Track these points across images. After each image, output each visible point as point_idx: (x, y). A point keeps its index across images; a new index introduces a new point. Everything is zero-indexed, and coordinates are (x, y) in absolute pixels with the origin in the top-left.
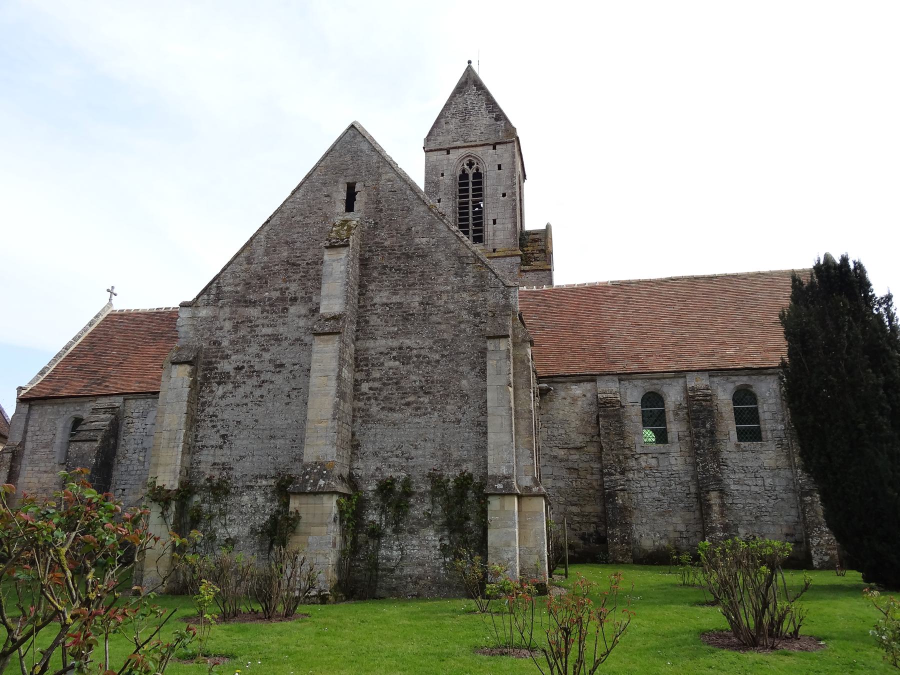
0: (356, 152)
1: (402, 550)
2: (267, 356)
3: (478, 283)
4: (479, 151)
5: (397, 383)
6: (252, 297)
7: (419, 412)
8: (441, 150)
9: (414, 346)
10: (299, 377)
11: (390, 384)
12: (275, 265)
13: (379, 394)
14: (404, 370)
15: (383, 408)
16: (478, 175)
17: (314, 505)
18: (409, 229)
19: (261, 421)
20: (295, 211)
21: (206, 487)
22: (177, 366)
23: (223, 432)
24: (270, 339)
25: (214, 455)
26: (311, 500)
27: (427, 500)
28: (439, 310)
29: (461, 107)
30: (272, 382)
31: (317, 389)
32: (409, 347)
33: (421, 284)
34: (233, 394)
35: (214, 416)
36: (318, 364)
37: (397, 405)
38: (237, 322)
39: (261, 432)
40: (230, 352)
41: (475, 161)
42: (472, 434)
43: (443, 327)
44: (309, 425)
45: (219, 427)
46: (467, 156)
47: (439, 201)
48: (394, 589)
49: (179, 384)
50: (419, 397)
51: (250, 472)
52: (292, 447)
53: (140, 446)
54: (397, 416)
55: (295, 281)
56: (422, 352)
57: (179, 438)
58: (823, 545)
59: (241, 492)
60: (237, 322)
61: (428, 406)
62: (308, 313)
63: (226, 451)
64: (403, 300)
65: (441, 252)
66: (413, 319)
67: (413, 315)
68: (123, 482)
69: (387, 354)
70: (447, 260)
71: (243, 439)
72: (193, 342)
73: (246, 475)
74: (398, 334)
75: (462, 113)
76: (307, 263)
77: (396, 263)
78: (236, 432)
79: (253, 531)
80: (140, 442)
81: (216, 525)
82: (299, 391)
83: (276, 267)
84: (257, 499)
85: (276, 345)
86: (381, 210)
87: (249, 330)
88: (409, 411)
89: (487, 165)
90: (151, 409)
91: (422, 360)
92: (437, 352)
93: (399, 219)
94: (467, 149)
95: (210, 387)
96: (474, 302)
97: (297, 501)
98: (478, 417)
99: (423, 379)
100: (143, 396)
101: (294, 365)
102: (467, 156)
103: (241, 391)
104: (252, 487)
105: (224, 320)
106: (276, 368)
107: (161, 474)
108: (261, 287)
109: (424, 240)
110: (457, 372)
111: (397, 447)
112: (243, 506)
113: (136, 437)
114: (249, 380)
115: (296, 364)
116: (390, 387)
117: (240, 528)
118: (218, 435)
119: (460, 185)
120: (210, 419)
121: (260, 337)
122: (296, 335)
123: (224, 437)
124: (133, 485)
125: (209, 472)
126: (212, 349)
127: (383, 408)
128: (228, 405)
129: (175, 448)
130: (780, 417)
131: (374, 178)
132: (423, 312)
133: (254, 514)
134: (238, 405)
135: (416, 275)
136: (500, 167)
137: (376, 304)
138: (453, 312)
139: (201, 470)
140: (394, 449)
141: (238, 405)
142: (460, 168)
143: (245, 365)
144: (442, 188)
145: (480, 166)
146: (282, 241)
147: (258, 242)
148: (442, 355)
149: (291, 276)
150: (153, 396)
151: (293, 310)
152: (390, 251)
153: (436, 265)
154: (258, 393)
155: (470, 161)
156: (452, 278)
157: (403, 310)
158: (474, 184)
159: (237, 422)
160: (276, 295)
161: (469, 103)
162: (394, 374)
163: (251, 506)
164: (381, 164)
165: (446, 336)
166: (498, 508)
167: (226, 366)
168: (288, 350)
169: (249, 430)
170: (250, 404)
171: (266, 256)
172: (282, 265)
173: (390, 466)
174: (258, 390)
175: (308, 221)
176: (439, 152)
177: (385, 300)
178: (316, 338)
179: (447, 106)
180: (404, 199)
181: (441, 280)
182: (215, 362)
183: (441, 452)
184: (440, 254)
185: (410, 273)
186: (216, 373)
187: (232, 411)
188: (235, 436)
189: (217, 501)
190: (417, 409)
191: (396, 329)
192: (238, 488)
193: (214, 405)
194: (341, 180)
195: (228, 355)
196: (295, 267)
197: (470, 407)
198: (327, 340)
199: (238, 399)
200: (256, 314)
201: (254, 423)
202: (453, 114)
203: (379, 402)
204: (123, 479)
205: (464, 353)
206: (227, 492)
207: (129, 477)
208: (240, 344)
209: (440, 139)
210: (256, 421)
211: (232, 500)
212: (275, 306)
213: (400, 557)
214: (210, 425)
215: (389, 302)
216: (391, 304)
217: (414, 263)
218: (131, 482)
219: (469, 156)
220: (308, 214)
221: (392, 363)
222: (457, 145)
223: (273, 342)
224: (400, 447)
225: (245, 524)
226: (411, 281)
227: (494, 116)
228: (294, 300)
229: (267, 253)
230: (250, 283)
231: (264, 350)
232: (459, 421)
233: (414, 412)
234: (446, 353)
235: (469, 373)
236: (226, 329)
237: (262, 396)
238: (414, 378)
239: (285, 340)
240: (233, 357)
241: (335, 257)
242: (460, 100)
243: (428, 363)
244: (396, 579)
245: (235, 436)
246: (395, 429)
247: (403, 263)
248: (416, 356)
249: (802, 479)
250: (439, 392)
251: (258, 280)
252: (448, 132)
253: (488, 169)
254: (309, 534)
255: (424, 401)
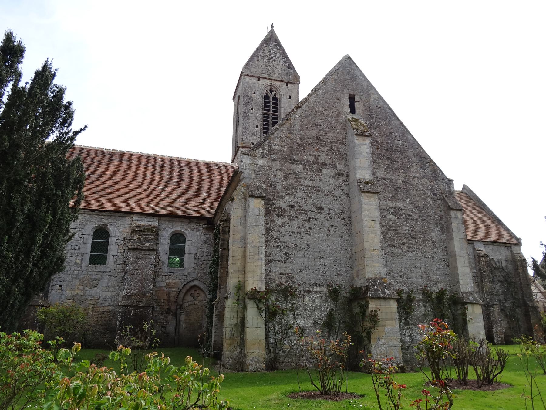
0: (353, 75)
1: (411, 336)
2: (310, 200)
3: (433, 175)
4: (278, 84)
5: (396, 230)
6: (295, 157)
7: (410, 250)
8: (254, 77)
9: (403, 207)
10: (334, 218)
11: (391, 230)
12: (309, 138)
13: (386, 236)
14: (398, 222)
15: (389, 245)
16: (275, 99)
17: (385, 307)
18: (391, 133)
19: (311, 246)
20: (317, 104)
21: (277, 290)
22: (254, 199)
23: (285, 251)
24: (311, 189)
25: (281, 267)
26: (382, 303)
27: (421, 305)
28: (414, 188)
29: (267, 53)
30: (316, 219)
31: (368, 229)
32: (400, 208)
33: (402, 169)
34: (290, 224)
35: (277, 239)
36: (366, 212)
37: (397, 244)
38: (286, 173)
39: (312, 253)
40: (283, 194)
41: (275, 90)
42: (441, 266)
43: (418, 198)
44: (366, 252)
45: (282, 247)
46: (270, 85)
47: (252, 109)
48: (409, 361)
49: (257, 212)
50: (409, 240)
51: (307, 281)
52: (335, 266)
53: (77, 251)
54: (397, 251)
55: (323, 152)
56: (408, 212)
57: (262, 253)
58: (498, 332)
59: (303, 295)
60: (286, 173)
61: (415, 247)
62: (335, 176)
63: (288, 264)
64: (393, 178)
65: (411, 152)
66: (400, 191)
67: (400, 188)
68: (60, 279)
69: (387, 210)
70: (415, 157)
71: (301, 257)
72: (255, 182)
73: (305, 283)
74: (392, 199)
75: (268, 57)
76: (330, 142)
77: (386, 153)
78: (294, 252)
79: (315, 323)
80: (77, 248)
81: (289, 318)
82: (335, 227)
83: (310, 140)
84: (315, 300)
85: (316, 193)
86: (373, 117)
87: (295, 180)
88: (404, 248)
89: (282, 94)
90: (88, 223)
91: (409, 218)
92: (416, 213)
93: (385, 126)
94: (270, 81)
95: (271, 217)
96: (432, 186)
97: (373, 304)
98: (442, 256)
99: (410, 229)
100: (98, 213)
101: (330, 209)
102: (270, 85)
103: (295, 223)
104: (311, 292)
105: (277, 170)
106: (318, 210)
107: (250, 278)
108: (301, 151)
109: (400, 142)
110: (428, 227)
111: (400, 270)
112: (306, 305)
113: (73, 244)
114: (300, 216)
115: (331, 209)
116: (392, 232)
117: (306, 320)
118: (282, 253)
119: (265, 102)
120: (275, 241)
121: (304, 187)
122: (329, 189)
123: (286, 254)
124: (71, 282)
125: (277, 279)
126: (269, 189)
127: (389, 245)
128: (287, 232)
129: (260, 260)
130: (474, 266)
131: (366, 95)
132: (405, 187)
133: (314, 310)
134: (294, 233)
135: (399, 164)
136: (290, 97)
137: (377, 177)
138: (422, 190)
139: (272, 277)
140: (399, 272)
141: (294, 233)
142: (265, 92)
143: (296, 204)
144: (254, 101)
145: (278, 94)
146: (312, 123)
147: (294, 119)
148: (419, 216)
149: (320, 148)
150: (92, 213)
151: (324, 171)
152: (381, 145)
153: (409, 159)
154: (307, 225)
155: (271, 88)
156: (419, 169)
157: (394, 184)
158: (273, 104)
159: (295, 245)
160: (312, 159)
161: (272, 52)
162: (393, 224)
163: (312, 305)
164: (369, 87)
165: (420, 204)
166: (471, 311)
167: (281, 203)
168: (324, 199)
169: (304, 251)
170: (302, 233)
171: (301, 130)
172: (314, 139)
173: (397, 282)
174: (307, 223)
175: (326, 112)
176: (253, 78)
177: (382, 176)
178: (363, 194)
179: (258, 50)
180: (386, 114)
181: (413, 169)
182: (273, 200)
183: (425, 276)
184: (410, 153)
185: (395, 161)
186: (275, 208)
187: (290, 237)
188: (295, 255)
189: (286, 300)
190: (409, 247)
191: (391, 195)
192: (300, 292)
193: (276, 230)
194: (346, 91)
195: (282, 196)
196: (322, 142)
197: (438, 250)
198: (371, 197)
199: (293, 229)
200: (299, 170)
201: (307, 246)
202: (262, 56)
203: (386, 241)
204: (60, 277)
205: (431, 217)
206: (293, 295)
207: (66, 275)
208: (291, 189)
209: (254, 69)
210: (308, 245)
211: (299, 300)
212: (312, 167)
213: (410, 340)
214: (275, 245)
215: (385, 177)
216: (386, 179)
217: (396, 155)
218: (68, 279)
219: (271, 85)
220: (327, 108)
221: (391, 217)
222: (264, 77)
223: (313, 191)
224: (402, 271)
225: (309, 318)
226: (396, 167)
227: (287, 65)
228: (325, 165)
229: (302, 128)
230: (293, 147)
231: (308, 196)
232: (433, 257)
233: (407, 249)
234: (421, 215)
235: (435, 229)
236: (278, 176)
237: (310, 228)
238: (405, 228)
239: (322, 191)
240: (286, 198)
241: (362, 142)
242: (266, 49)
243: (412, 219)
244: (409, 354)
245: (295, 255)
246: (397, 259)
247: (390, 154)
248: (405, 214)
249: (488, 299)
250: (420, 238)
251: (298, 146)
252: (259, 67)
253: (283, 97)
254: (385, 326)
255: (412, 243)
